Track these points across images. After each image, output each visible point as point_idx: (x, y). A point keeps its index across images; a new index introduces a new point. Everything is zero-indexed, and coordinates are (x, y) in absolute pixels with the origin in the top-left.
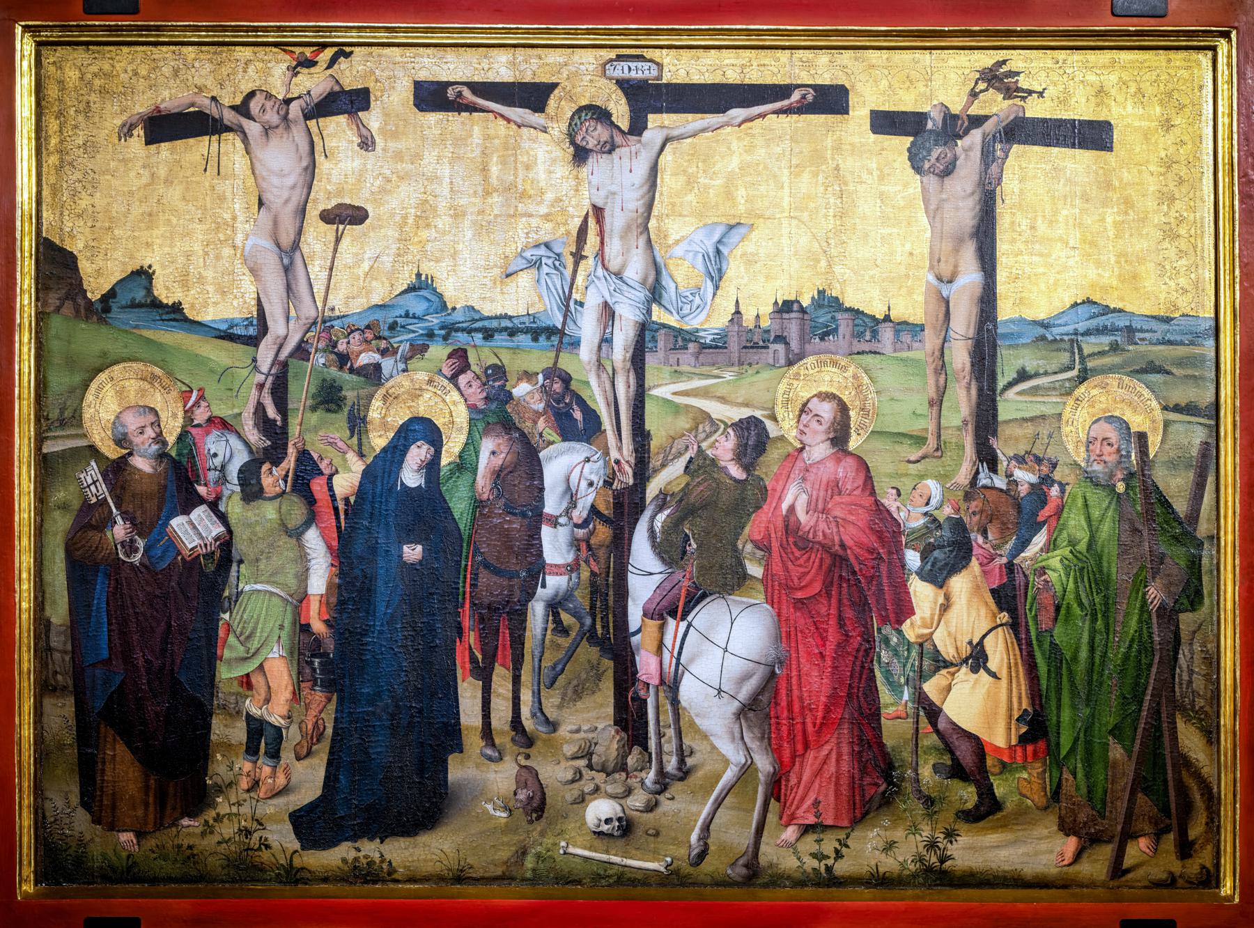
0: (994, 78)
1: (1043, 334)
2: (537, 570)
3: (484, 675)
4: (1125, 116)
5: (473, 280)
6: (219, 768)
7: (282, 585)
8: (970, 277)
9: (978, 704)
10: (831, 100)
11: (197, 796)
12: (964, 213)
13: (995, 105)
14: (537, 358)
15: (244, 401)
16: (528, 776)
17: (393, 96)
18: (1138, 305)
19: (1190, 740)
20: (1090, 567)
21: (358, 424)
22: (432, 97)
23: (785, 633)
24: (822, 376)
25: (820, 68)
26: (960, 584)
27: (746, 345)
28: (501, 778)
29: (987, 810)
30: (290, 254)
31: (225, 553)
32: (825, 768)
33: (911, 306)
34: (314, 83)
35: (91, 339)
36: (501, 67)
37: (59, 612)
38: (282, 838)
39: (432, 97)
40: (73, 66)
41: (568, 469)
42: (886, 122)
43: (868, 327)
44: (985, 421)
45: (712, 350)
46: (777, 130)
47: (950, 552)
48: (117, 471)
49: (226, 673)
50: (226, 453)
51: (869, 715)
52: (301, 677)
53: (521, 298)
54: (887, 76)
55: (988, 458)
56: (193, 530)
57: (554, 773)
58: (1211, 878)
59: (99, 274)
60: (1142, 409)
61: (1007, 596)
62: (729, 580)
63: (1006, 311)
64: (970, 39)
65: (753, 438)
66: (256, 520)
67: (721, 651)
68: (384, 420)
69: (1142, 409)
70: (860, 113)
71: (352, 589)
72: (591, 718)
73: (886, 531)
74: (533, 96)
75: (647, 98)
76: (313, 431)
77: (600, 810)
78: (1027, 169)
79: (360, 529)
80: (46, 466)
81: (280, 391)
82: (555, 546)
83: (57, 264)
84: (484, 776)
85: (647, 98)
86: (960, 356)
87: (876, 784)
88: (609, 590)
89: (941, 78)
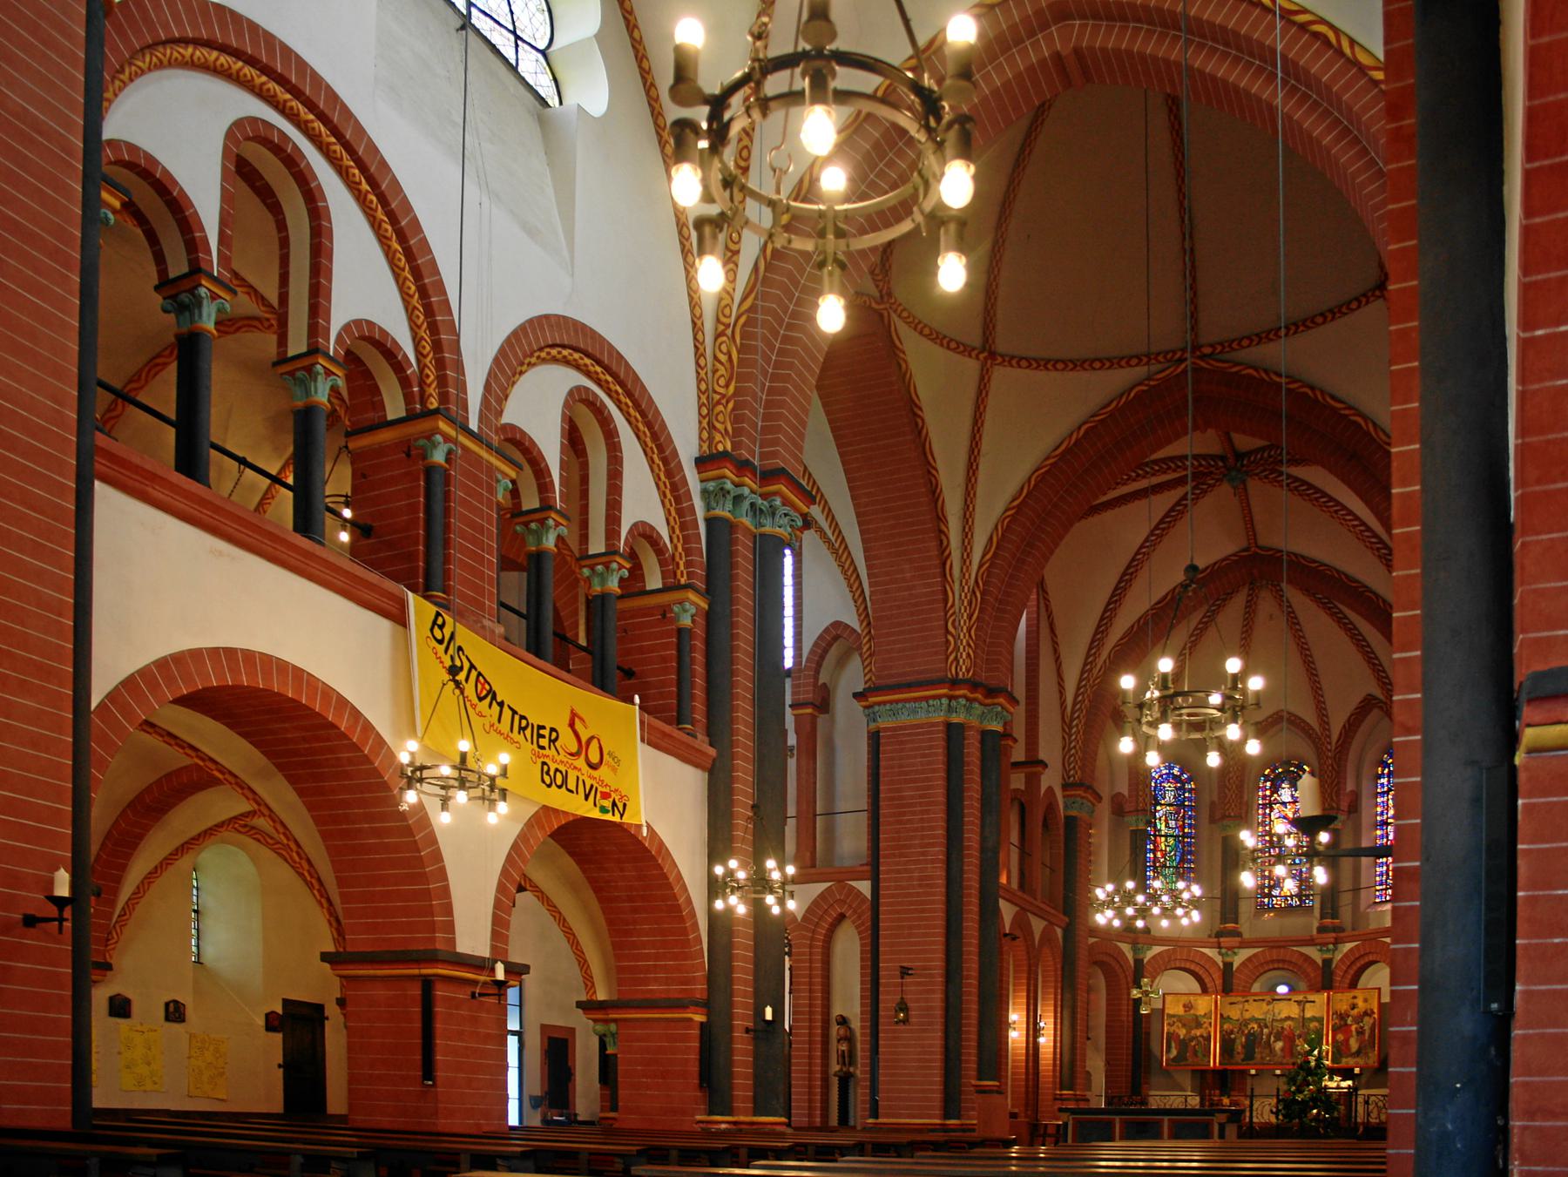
5: (1258, 1015)
27: (1283, 1020)
67: (1279, 1045)
84: (1258, 1056)
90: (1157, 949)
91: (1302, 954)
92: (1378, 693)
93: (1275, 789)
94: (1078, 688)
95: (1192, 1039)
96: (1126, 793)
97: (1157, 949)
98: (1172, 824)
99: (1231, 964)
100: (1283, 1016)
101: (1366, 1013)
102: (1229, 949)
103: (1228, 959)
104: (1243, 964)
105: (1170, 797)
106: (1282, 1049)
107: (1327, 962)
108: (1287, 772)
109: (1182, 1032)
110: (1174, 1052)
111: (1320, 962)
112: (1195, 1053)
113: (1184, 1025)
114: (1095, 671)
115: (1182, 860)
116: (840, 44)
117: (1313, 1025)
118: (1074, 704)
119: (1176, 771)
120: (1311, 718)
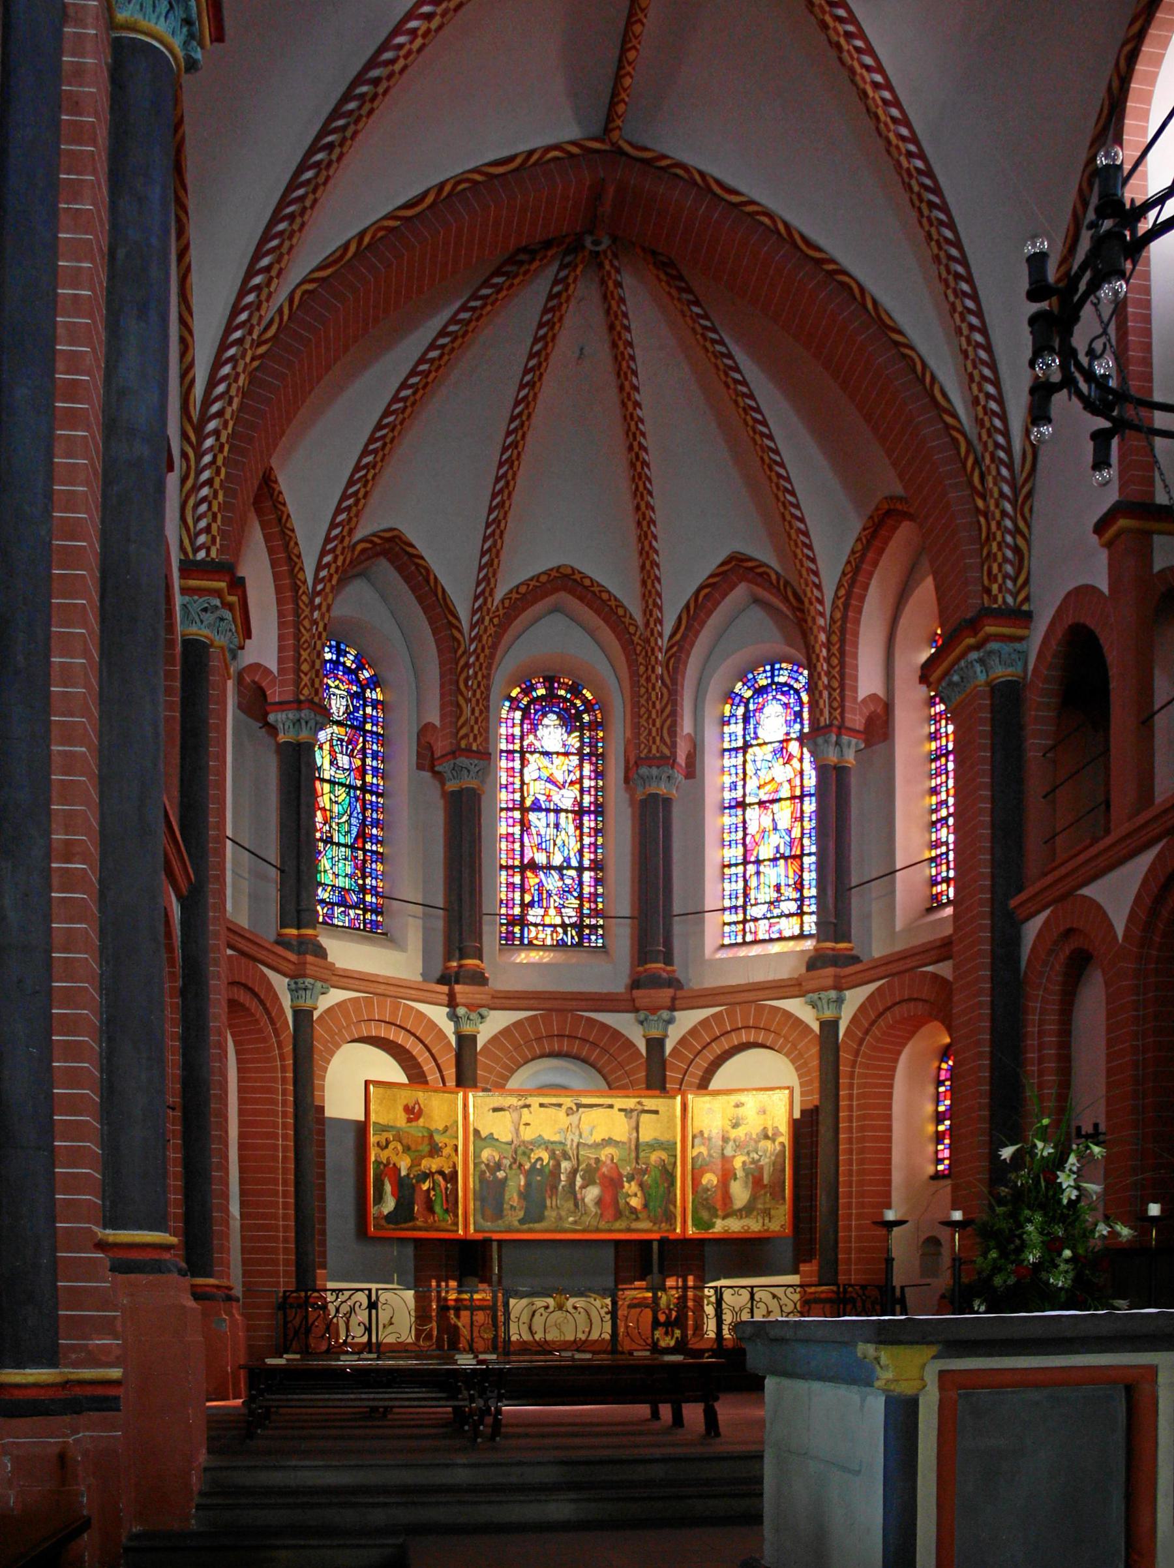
0: (639, 1103)
1: (647, 1144)
2: (560, 1180)
3: (551, 1198)
4: (661, 1109)
5: (550, 1135)
6: (505, 1213)
8: (635, 1134)
9: (635, 1202)
10: (611, 1106)
12: (634, 1124)
13: (639, 1107)
14: (561, 1147)
15: (510, 1154)
16: (558, 1214)
19: (672, 1207)
20: (655, 1181)
21: (529, 1158)
22: (541, 1105)
23: (603, 1191)
25: (609, 1101)
26: (633, 1183)
27: (597, 1146)
28: (554, 1214)
29: (637, 1219)
31: (506, 1178)
32: (610, 1213)
34: (521, 1103)
36: (554, 1100)
37: (477, 1188)
38: (516, 1223)
39: (541, 1105)
41: (565, 1165)
42: (620, 1110)
44: (637, 1158)
45: (590, 1146)
46: (601, 1110)
47: (631, 1178)
48: (487, 1165)
49: (507, 1197)
50: (507, 1162)
51: (617, 1203)
52: (520, 1197)
53: (556, 1138)
54: (619, 1103)
55: (637, 1163)
56: (501, 1174)
57: (563, 1213)
58: (675, 1229)
59: (484, 1134)
60: (664, 1155)
61: (641, 1185)
63: (641, 1140)
64: (634, 1097)
65: (597, 1160)
66: (511, 1173)
67: (592, 1193)
68: (534, 1157)
69: (664, 1155)
70: (616, 1108)
72: (570, 1205)
73: (620, 1176)
74: (560, 1105)
75: (579, 1106)
76: (523, 1160)
77: (571, 1219)
78: (645, 1118)
80: (475, 1165)
81: (516, 1152)
82: (563, 1177)
83: (477, 1132)
84: (550, 1214)
85: (579, 1106)
86: (633, 1147)
87: (618, 1215)
89: (630, 1103)
90: (336, 996)
91: (605, 1027)
92: (764, 553)
93: (531, 722)
94: (223, 346)
95: (426, 1176)
96: (273, 666)
97: (336, 996)
98: (343, 761)
99: (473, 1038)
100: (598, 1137)
102: (471, 1007)
103: (467, 1029)
104: (494, 1040)
106: (599, 1202)
107: (829, 1026)
108: (551, 697)
110: (389, 1205)
111: (816, 1027)
112: (429, 1207)
113: (407, 1149)
114: (269, 311)
115: (362, 835)
117: (655, 1157)
118: (212, 383)
119: (349, 661)
120: (621, 585)
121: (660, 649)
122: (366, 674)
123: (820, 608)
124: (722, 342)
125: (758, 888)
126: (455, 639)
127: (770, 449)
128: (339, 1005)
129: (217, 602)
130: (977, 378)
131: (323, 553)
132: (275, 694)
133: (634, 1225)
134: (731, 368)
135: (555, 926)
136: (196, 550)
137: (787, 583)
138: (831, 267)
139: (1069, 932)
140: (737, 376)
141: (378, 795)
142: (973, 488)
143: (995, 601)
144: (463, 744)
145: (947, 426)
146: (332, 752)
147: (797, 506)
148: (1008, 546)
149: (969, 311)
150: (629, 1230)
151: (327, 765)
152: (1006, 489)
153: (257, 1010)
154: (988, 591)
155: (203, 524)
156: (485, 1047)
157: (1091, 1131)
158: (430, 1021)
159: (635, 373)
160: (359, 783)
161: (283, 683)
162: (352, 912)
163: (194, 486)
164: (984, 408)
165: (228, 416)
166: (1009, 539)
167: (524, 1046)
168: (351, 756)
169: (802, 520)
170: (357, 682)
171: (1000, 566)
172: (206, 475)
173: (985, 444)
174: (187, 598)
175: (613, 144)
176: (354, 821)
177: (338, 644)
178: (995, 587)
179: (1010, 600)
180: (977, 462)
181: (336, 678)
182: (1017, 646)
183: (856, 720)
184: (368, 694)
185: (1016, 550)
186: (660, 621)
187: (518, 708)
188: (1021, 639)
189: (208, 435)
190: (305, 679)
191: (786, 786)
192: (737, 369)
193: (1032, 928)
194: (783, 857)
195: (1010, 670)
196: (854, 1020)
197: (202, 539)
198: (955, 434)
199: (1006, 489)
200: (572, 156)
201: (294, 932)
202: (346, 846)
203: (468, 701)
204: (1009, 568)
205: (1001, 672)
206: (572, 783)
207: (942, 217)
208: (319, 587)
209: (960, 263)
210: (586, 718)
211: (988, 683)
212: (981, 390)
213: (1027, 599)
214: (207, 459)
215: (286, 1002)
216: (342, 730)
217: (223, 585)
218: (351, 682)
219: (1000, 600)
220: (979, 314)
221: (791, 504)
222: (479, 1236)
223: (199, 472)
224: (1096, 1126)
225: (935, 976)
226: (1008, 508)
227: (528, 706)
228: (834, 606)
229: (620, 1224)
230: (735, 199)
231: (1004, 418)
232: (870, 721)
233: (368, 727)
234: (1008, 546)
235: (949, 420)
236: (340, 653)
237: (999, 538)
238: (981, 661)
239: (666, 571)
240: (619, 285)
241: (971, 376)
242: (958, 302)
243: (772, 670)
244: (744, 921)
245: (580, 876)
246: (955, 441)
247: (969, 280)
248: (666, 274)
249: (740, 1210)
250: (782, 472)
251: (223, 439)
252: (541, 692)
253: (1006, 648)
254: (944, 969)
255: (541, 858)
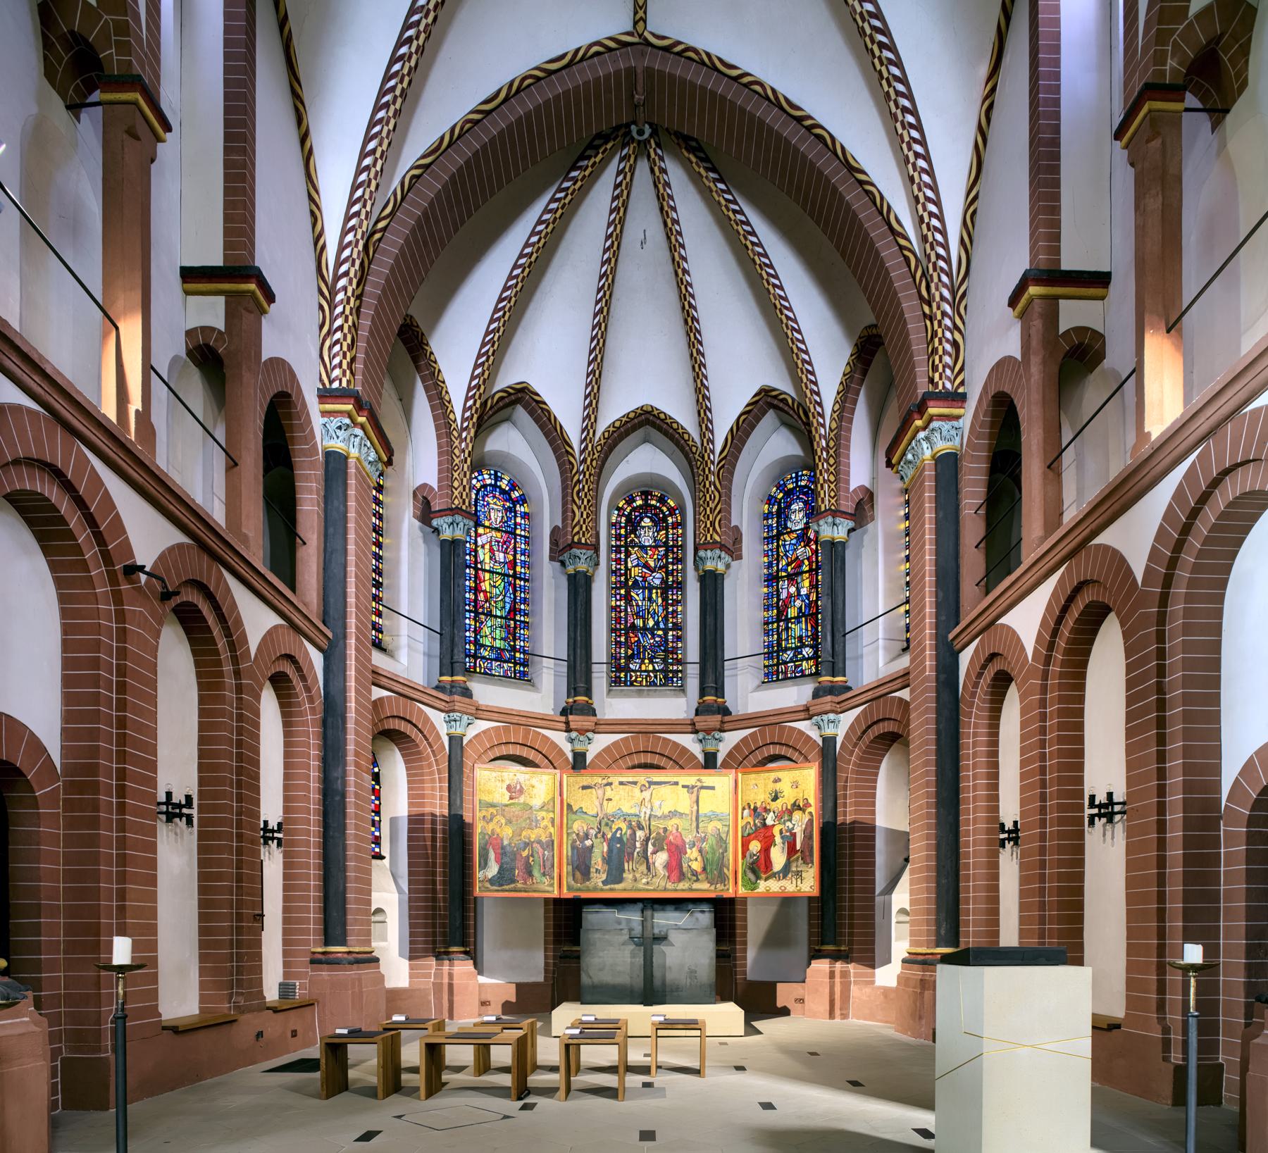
1: (705, 815)
5: (627, 809)
7: (601, 849)
9: (696, 866)
10: (676, 783)
11: (589, 879)
15: (595, 825)
17: (616, 783)
18: (718, 811)
22: (621, 783)
24: (675, 821)
27: (664, 817)
28: (631, 876)
29: (698, 880)
30: (601, 805)
32: (675, 874)
33: (687, 812)
34: (605, 782)
35: (574, 817)
36: (630, 779)
39: (621, 783)
40: (572, 779)
41: (640, 834)
43: (681, 814)
44: (697, 827)
45: (659, 818)
46: (669, 787)
51: (681, 867)
56: (588, 843)
57: (638, 876)
61: (700, 851)
62: (662, 849)
65: (665, 830)
66: (597, 842)
67: (661, 859)
68: (615, 827)
71: (610, 850)
72: (643, 868)
74: (635, 783)
76: (604, 829)
77: (644, 881)
78: (703, 792)
79: (610, 843)
82: (638, 845)
85: (651, 783)
87: (682, 877)
88: (645, 851)
90: (482, 725)
92: (783, 385)
96: (435, 486)
98: (500, 556)
101: (796, 807)
103: (579, 748)
104: (599, 756)
105: (496, 517)
109: (507, 833)
111: (821, 743)
116: (443, 715)
120: (684, 417)
121: (713, 463)
122: (515, 495)
123: (821, 420)
124: (741, 212)
125: (787, 640)
126: (571, 463)
127: (781, 297)
128: (484, 732)
129: (347, 421)
130: (922, 200)
131: (467, 399)
132: (436, 506)
133: (696, 886)
134: (749, 233)
135: (648, 672)
136: (331, 382)
137: (799, 404)
138: (809, 122)
139: (993, 656)
140: (754, 239)
141: (526, 580)
142: (921, 297)
143: (937, 387)
144: (576, 539)
145: (901, 248)
146: (491, 550)
147: (803, 342)
148: (948, 341)
149: (915, 141)
150: (691, 890)
151: (487, 560)
152: (946, 293)
153: (412, 732)
154: (931, 380)
155: (336, 361)
156: (592, 761)
157: (1104, 801)
158: (553, 743)
159: (683, 246)
160: (511, 572)
161: (441, 497)
162: (505, 665)
163: (329, 333)
164: (928, 225)
165: (352, 274)
166: (948, 335)
167: (613, 760)
168: (505, 552)
169: (806, 352)
170: (510, 499)
171: (941, 358)
172: (338, 322)
173: (929, 257)
174: (326, 419)
175: (640, 36)
176: (507, 600)
177: (496, 472)
178: (937, 376)
179: (948, 385)
180: (923, 274)
181: (494, 497)
182: (955, 423)
183: (848, 506)
184: (518, 508)
185: (955, 344)
186: (711, 441)
187: (624, 515)
188: (957, 418)
189: (339, 291)
190: (456, 493)
191: (806, 562)
192: (753, 233)
193: (965, 658)
194: (804, 615)
195: (949, 444)
196: (847, 736)
197: (337, 372)
198: (906, 253)
199: (946, 293)
200: (610, 50)
201: (449, 679)
202: (501, 617)
203: (579, 508)
204: (947, 359)
205: (942, 446)
206: (661, 568)
207: (890, 55)
208: (465, 424)
209: (907, 98)
210: (670, 520)
211: (933, 457)
212: (925, 209)
213: (962, 383)
214: (339, 310)
215: (443, 730)
216: (499, 535)
217: (350, 407)
218: (507, 500)
219: (940, 387)
220: (923, 143)
221: (798, 340)
222: (571, 895)
223: (332, 321)
224: (1110, 795)
225: (901, 700)
226: (948, 309)
227: (630, 514)
228: (832, 419)
229: (683, 885)
230: (734, 73)
231: (944, 233)
232: (859, 505)
233: (518, 532)
234: (948, 341)
235: (902, 242)
236: (497, 478)
237: (940, 335)
238: (927, 439)
239: (715, 403)
240: (664, 171)
241: (917, 199)
242: (905, 133)
243: (797, 476)
244: (778, 664)
245: (666, 634)
246: (907, 259)
247: (914, 113)
248: (696, 157)
249: (778, 873)
250: (790, 315)
251: (349, 294)
252: (639, 502)
253: (946, 426)
254: (905, 694)
255: (639, 623)
